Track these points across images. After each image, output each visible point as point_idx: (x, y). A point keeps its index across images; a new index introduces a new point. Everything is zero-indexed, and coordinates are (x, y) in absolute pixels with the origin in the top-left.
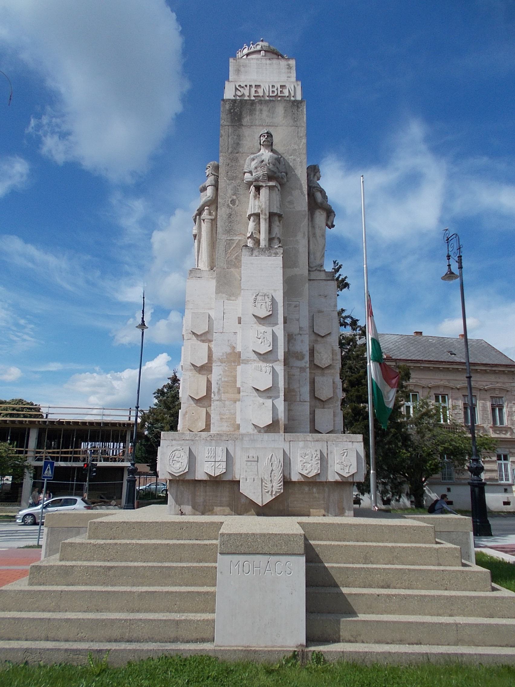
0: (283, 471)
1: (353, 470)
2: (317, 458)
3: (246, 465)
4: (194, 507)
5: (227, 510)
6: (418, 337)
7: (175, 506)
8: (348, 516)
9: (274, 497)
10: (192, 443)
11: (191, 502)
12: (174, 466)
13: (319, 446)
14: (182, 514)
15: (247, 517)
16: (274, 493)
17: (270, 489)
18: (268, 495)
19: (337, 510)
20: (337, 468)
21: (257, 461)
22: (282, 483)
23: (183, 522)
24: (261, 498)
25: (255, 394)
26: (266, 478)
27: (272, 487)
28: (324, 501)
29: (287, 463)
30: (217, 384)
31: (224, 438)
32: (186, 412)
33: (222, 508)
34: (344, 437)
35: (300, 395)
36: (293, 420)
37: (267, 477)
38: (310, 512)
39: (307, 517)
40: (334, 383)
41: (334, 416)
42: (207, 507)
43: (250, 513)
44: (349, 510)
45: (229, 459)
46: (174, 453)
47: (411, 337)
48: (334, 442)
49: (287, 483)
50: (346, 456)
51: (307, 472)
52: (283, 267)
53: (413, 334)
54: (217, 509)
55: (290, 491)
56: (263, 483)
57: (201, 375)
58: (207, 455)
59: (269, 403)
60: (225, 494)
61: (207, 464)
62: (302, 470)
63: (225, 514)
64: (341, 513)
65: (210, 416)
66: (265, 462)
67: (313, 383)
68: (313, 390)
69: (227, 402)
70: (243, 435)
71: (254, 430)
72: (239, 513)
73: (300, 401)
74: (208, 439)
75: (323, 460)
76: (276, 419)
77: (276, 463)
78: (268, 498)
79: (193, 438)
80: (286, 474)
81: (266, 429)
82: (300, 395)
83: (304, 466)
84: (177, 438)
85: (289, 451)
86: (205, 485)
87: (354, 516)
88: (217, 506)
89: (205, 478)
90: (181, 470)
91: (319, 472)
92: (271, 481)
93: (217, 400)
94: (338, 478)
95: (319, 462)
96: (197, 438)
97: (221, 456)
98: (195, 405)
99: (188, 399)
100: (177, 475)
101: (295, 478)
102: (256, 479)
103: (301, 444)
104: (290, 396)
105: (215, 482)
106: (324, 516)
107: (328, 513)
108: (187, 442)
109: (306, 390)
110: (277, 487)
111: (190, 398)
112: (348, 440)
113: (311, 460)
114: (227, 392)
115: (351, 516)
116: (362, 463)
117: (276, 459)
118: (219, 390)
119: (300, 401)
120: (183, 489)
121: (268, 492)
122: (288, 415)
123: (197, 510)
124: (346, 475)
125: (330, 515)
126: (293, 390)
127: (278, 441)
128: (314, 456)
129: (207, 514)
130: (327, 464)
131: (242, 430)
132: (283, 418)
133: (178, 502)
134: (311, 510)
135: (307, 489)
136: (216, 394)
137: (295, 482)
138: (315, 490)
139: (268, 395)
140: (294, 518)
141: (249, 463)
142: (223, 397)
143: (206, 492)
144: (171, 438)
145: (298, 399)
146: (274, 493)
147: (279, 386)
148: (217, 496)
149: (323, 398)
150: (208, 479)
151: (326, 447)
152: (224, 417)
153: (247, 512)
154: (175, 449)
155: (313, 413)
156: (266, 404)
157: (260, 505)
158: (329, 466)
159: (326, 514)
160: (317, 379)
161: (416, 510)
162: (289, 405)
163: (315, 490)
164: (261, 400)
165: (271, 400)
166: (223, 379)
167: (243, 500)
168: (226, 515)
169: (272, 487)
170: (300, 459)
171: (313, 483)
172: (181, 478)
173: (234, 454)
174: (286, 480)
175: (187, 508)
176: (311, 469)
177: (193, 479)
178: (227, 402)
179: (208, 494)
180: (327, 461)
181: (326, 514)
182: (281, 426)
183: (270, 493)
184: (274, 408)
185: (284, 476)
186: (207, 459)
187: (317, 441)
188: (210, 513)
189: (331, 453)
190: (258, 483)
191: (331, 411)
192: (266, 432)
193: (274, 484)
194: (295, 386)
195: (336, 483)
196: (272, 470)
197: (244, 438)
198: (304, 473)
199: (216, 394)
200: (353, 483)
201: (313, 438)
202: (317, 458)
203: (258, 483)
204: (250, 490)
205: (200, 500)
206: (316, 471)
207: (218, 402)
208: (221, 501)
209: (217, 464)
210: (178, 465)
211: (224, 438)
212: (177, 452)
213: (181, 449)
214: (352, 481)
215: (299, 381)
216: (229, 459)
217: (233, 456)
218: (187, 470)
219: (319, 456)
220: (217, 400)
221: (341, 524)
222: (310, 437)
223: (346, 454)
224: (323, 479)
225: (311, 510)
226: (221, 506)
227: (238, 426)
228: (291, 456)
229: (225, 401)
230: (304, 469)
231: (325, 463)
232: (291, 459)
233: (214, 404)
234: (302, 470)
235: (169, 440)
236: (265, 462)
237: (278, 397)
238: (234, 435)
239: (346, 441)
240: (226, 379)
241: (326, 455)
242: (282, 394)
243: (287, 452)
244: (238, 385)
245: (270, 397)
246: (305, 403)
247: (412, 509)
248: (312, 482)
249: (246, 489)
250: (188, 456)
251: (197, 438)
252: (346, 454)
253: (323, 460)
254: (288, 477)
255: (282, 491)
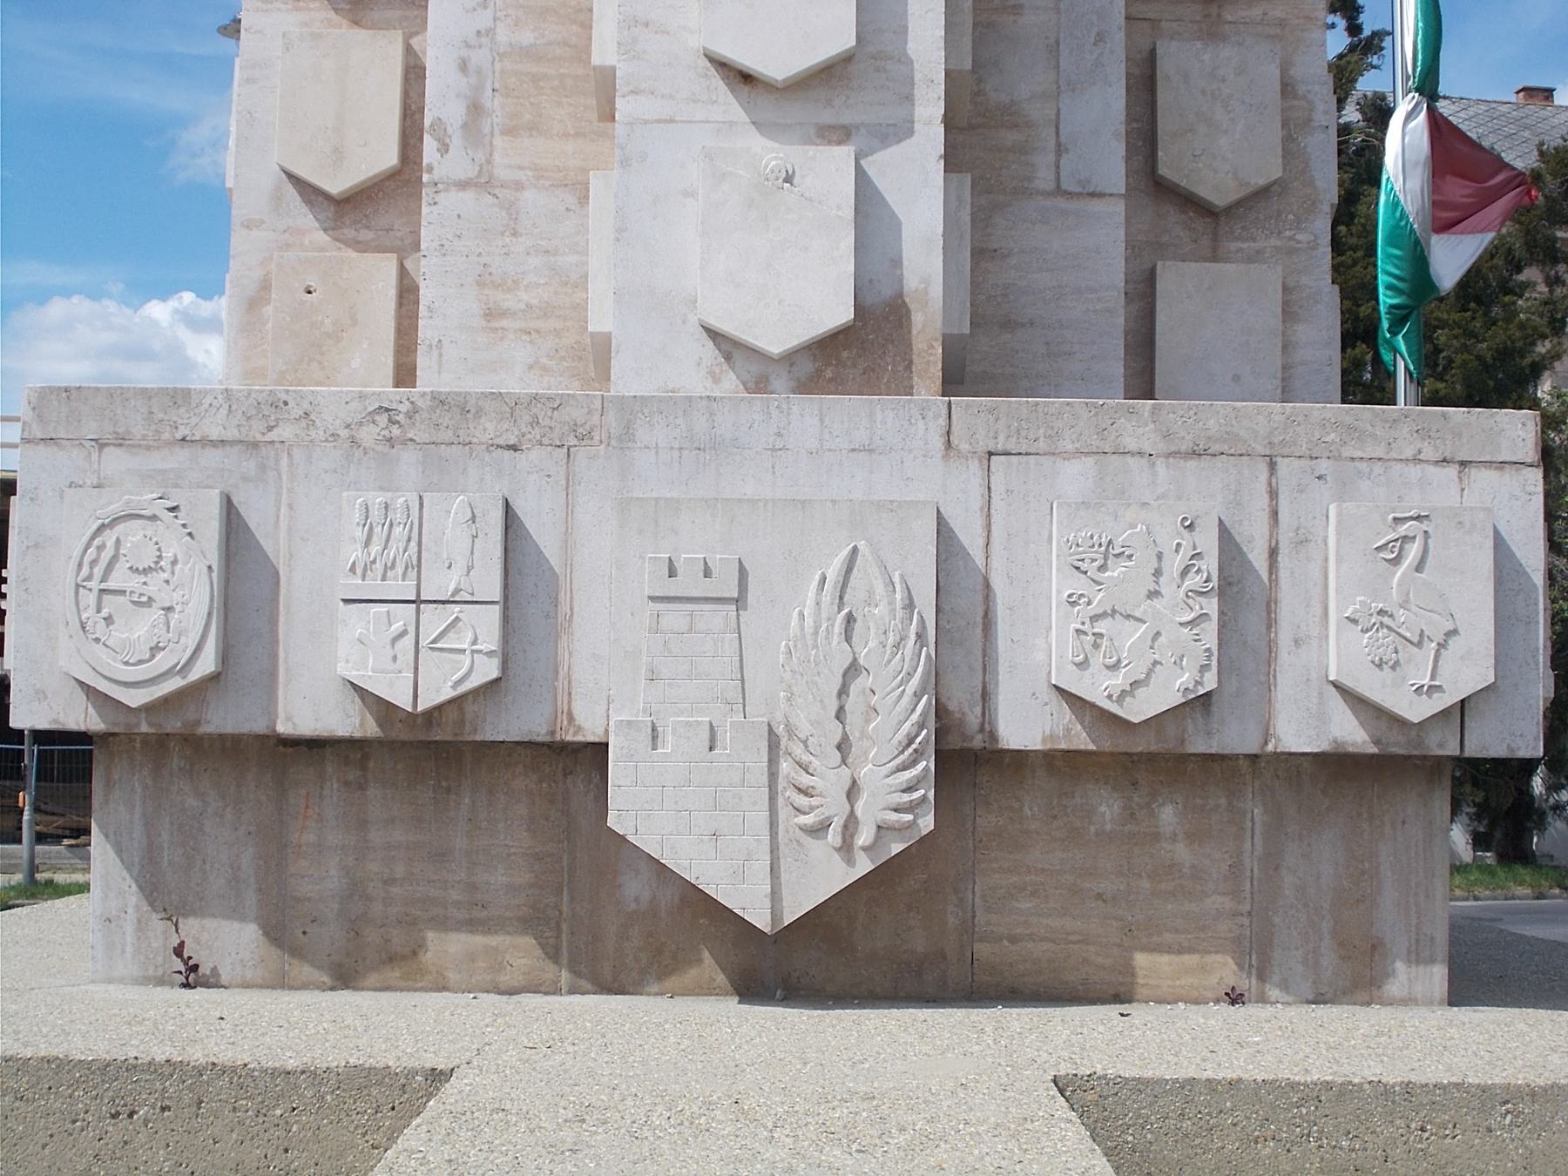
0: (937, 677)
1: (1469, 671)
2: (1194, 581)
3: (656, 629)
4: (276, 933)
5: (521, 953)
6: (1535, 109)
7: (141, 926)
8: (1408, 1001)
9: (864, 866)
10: (250, 466)
11: (251, 899)
12: (117, 635)
13: (1208, 492)
14: (192, 976)
15: (663, 1002)
16: (864, 837)
17: (836, 808)
18: (822, 851)
19: (1329, 960)
20: (1345, 654)
21: (740, 602)
22: (927, 764)
23: (131, 1067)
24: (768, 877)
25: (727, 104)
26: (804, 729)
27: (852, 792)
28: (1235, 894)
29: (962, 615)
30: (464, 66)
31: (488, 428)
32: (265, 286)
33: (479, 940)
34: (1405, 430)
35: (1060, 149)
36: (1008, 325)
37: (810, 717)
38: (1129, 970)
39: (1113, 1010)
40: (1287, 88)
41: (1289, 313)
42: (372, 935)
43: (692, 974)
44: (1417, 957)
45: (526, 584)
46: (109, 538)
47: (1504, 108)
48: (1323, 466)
49: (965, 761)
50: (1419, 568)
51: (1119, 681)
52: (913, 122)
53: (1513, 98)
54: (446, 947)
55: (988, 821)
56: (785, 766)
57: (362, 34)
58: (355, 554)
59: (830, 171)
60: (499, 841)
61: (358, 622)
62: (1083, 665)
63: (506, 979)
64: (1356, 977)
65: (415, 289)
66: (794, 610)
67: (1144, 84)
68: (1144, 136)
69: (532, 200)
70: (632, 408)
71: (716, 380)
72: (609, 976)
73: (1059, 191)
74: (368, 435)
75: (1242, 595)
76: (887, 293)
77: (879, 617)
78: (820, 878)
79: (256, 432)
80: (962, 700)
81: (807, 366)
82: (1060, 149)
83: (1098, 633)
84: (138, 430)
85: (979, 531)
86: (353, 775)
87: (1451, 1004)
88: (444, 924)
89: (344, 721)
90: (163, 662)
91: (1210, 682)
92: (843, 746)
93: (463, 185)
94: (1351, 733)
95: (1212, 606)
96: (285, 432)
97: (465, 560)
98: (322, 237)
99: (277, 198)
100: (135, 698)
101: (1024, 724)
102: (726, 736)
103: (1074, 476)
104: (980, 137)
105: (425, 754)
106: (1235, 998)
107: (1262, 978)
108: (212, 457)
109: (1100, 113)
110: (888, 791)
111: (290, 190)
112: (1429, 453)
113: (1154, 594)
114: (534, 128)
115: (1429, 1002)
116: (1530, 622)
117: (880, 588)
118: (476, 109)
119: (1059, 191)
120: (192, 802)
121: (819, 830)
122: (975, 285)
123: (297, 952)
124: (1416, 710)
125: (1274, 993)
126: (1009, 116)
127: (901, 456)
128: (1175, 564)
129: (373, 979)
130: (1271, 622)
131: (627, 380)
132: (937, 291)
133: (166, 895)
134: (1141, 959)
135: (1107, 807)
136: (456, 142)
137: (1020, 756)
138: (1168, 815)
139: (827, 117)
140: (1018, 1018)
141: (675, 617)
142: (507, 157)
143: (363, 824)
144: (91, 429)
145: (1044, 178)
146: (864, 837)
147: (912, 47)
148: (441, 856)
149: (1216, 187)
150: (372, 729)
151: (1263, 501)
152: (509, 301)
153: (664, 973)
154: (116, 508)
155: (1143, 294)
156: (805, 182)
157: (761, 920)
158: (1284, 637)
159: (1245, 984)
160: (1176, 57)
161: (1501, 873)
162: (982, 219)
163: (1168, 815)
164: (770, 153)
165: (843, 155)
166: (503, 36)
167: (635, 888)
168: (512, 992)
169: (852, 792)
170: (1060, 584)
171: (1154, 765)
172: (173, 725)
173: (567, 545)
174: (954, 742)
175: (230, 940)
176: (1152, 665)
177: (259, 727)
178: (529, 196)
179: (376, 836)
180: (1270, 607)
181: (1245, 984)
182: (919, 344)
183: (834, 836)
184: (870, 212)
185: (941, 711)
186: (356, 586)
187: (1195, 454)
188: (393, 975)
189: (1302, 542)
190: (744, 758)
191: (1270, 277)
192: (807, 386)
193: (865, 772)
194: (1023, 82)
195: (1336, 767)
196: (853, 669)
197: (642, 434)
198: (1099, 688)
199: (456, 142)
200: (1431, 767)
201: (1167, 436)
202: (1194, 581)
203: (744, 758)
204: (685, 814)
205: (320, 878)
206: (1185, 679)
207: (468, 196)
208: (472, 887)
209: (434, 621)
210: (139, 629)
211: (488, 428)
212: (132, 534)
213: (159, 508)
214: (1452, 749)
215: (1054, 49)
216: (526, 584)
217: (555, 561)
218: (206, 665)
219: (1211, 564)
220: (463, 185)
221: (1408, 1088)
222: (1138, 423)
223: (1413, 551)
224: (1235, 737)
225: (1141, 959)
226: (472, 925)
227: (601, 352)
228: (996, 563)
229: (519, 186)
230: (1097, 660)
231: (1252, 621)
232: (997, 583)
233: (441, 215)
234: (1083, 665)
235: (78, 442)
236: (794, 610)
237: (902, 130)
238: (579, 415)
239: (1416, 460)
240: (526, 37)
241: (1258, 558)
242: (930, 109)
243: (969, 536)
244: (604, 52)
245: (839, 134)
246: (1097, 206)
247: (1478, 865)
248: (1150, 758)
249: (639, 807)
250: (214, 558)
251: (285, 432)
252: (1413, 551)
253: (1242, 595)
254: (973, 719)
255: (927, 823)
